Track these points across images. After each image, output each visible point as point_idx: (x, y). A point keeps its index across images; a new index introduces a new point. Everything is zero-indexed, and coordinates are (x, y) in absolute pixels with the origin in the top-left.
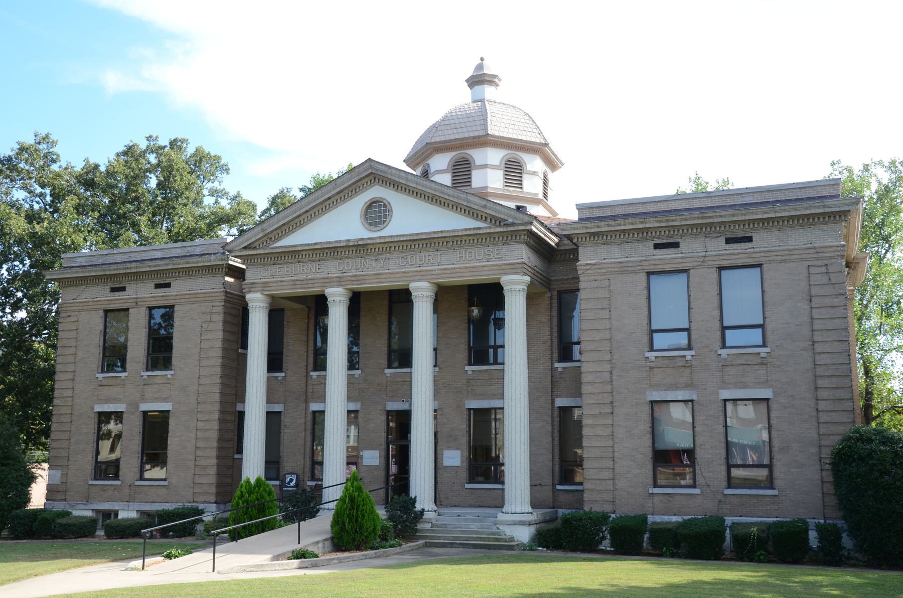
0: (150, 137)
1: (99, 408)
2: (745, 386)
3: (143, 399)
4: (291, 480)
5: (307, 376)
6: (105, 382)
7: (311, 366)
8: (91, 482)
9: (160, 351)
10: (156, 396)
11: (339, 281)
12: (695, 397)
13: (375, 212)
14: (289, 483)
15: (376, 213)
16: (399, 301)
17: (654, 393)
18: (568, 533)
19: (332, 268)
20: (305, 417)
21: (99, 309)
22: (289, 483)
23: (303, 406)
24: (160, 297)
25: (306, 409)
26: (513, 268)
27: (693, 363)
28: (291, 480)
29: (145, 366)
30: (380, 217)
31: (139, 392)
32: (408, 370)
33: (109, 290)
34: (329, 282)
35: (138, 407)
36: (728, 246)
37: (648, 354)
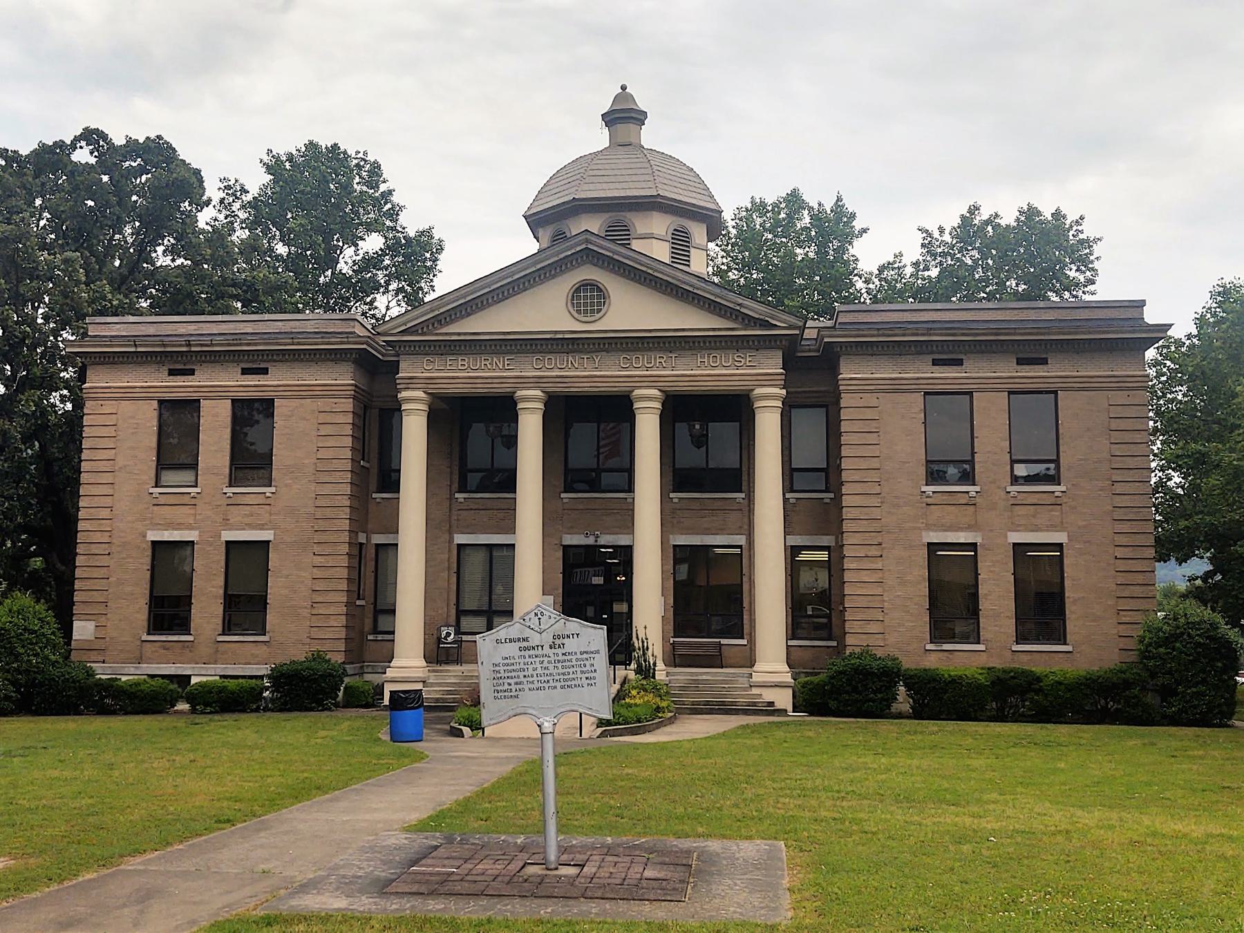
0: (638, 118)
1: (153, 536)
2: (1037, 529)
3: (227, 524)
4: (448, 634)
5: (451, 498)
6: (162, 500)
7: (456, 486)
8: (145, 637)
9: (250, 462)
10: (247, 520)
11: (652, 381)
12: (979, 540)
13: (585, 297)
14: (445, 638)
15: (589, 298)
16: (615, 410)
17: (931, 534)
18: (845, 690)
19: (528, 368)
20: (450, 551)
21: (151, 399)
22: (445, 638)
23: (447, 536)
24: (251, 386)
25: (451, 540)
26: (767, 380)
27: (978, 500)
28: (448, 634)
29: (227, 480)
30: (592, 304)
31: (209, 513)
32: (394, 495)
33: (166, 373)
34: (525, 382)
35: (145, 536)
36: (1019, 367)
37: (924, 488)
